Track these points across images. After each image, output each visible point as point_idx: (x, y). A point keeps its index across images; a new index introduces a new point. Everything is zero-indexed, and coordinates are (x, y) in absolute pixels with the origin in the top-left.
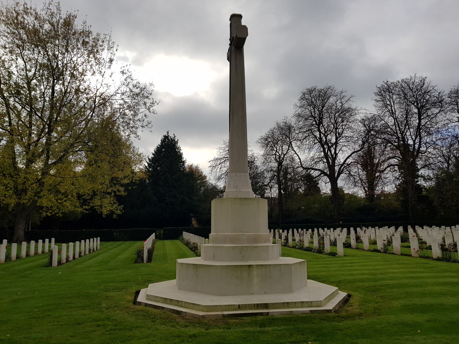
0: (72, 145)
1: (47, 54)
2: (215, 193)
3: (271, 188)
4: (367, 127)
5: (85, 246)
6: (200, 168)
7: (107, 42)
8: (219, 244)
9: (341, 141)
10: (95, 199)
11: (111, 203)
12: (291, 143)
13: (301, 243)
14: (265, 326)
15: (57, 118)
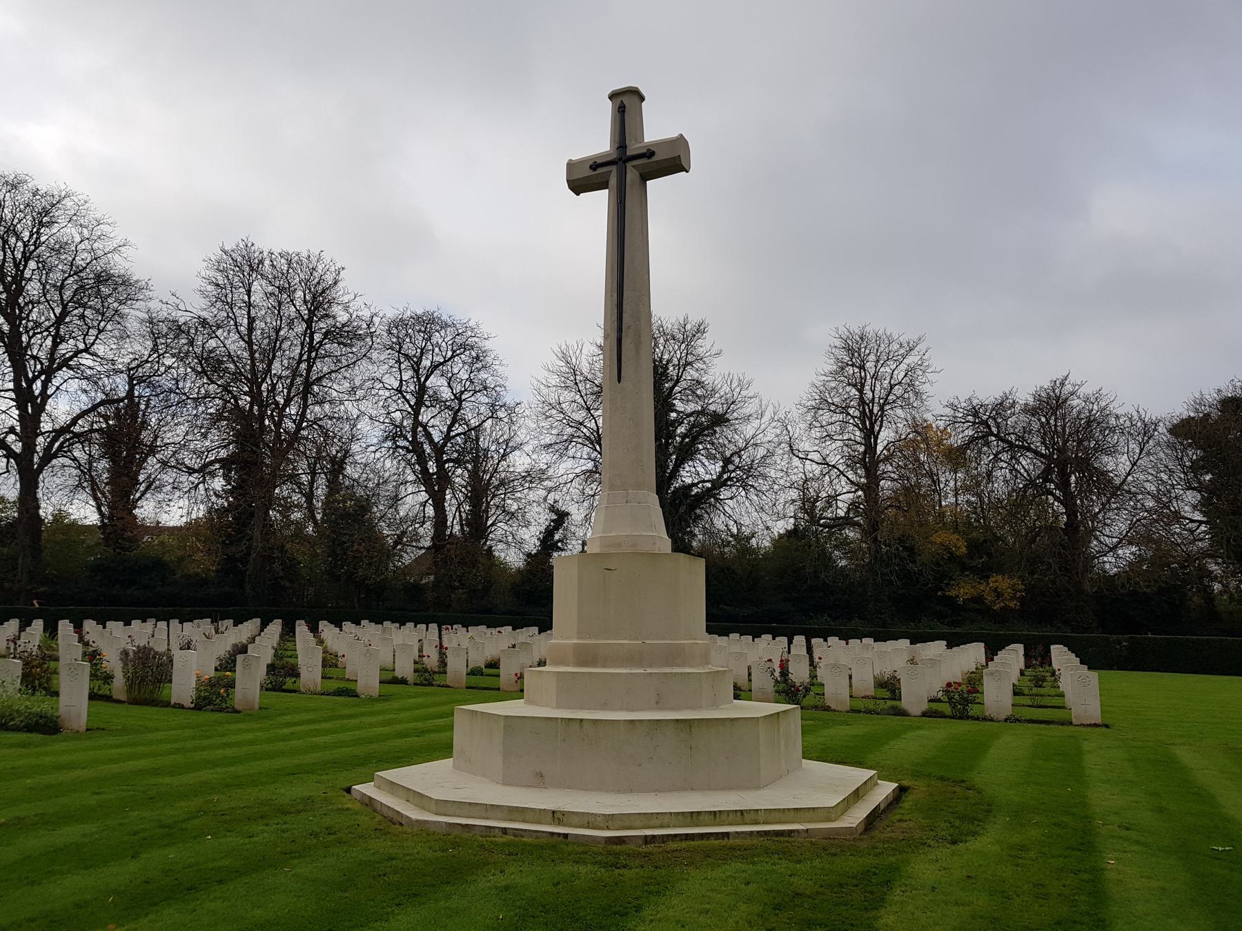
8: (604, 667)
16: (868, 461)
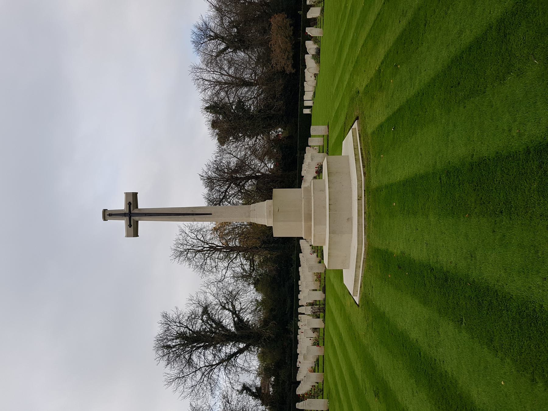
16: (228, 251)
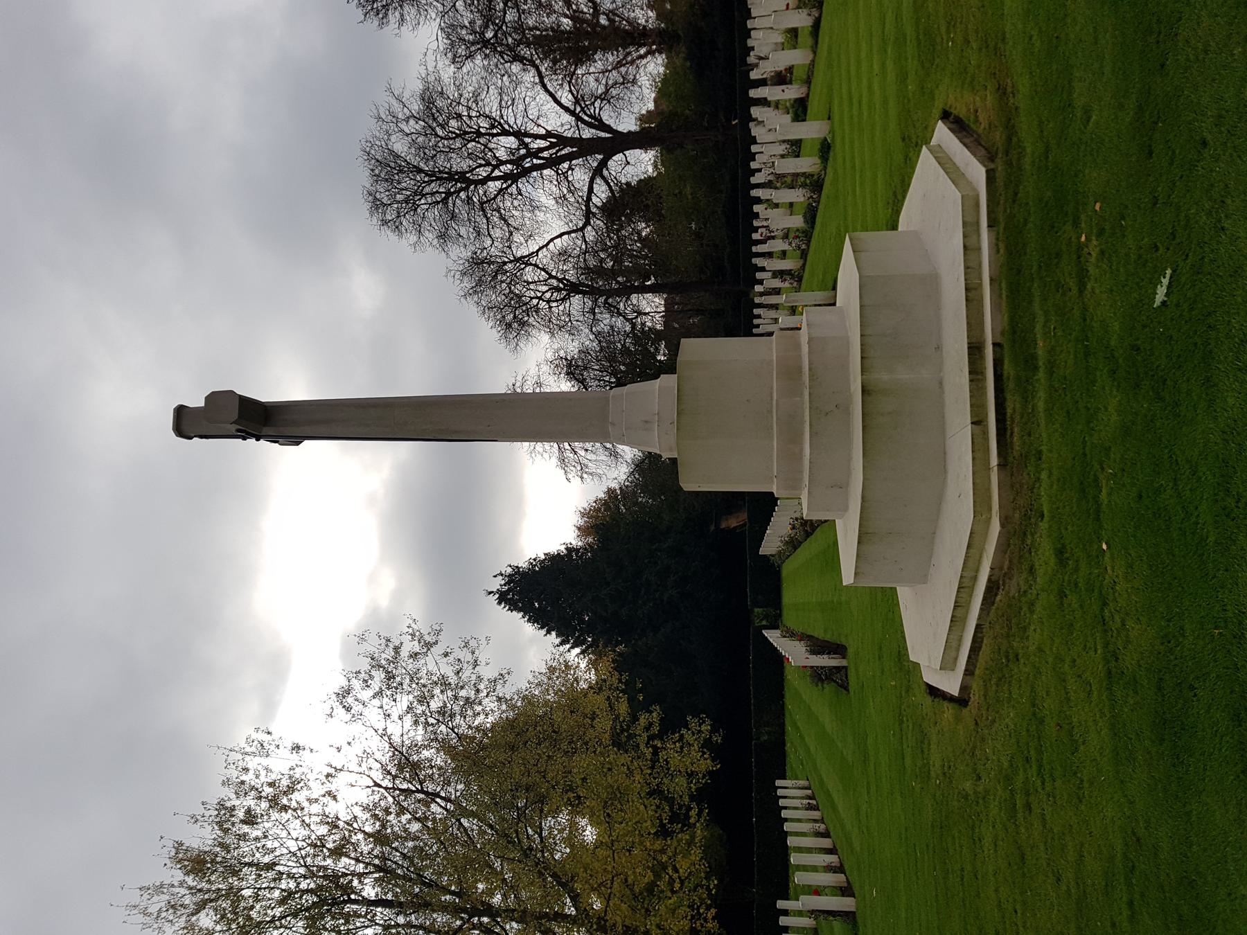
0: (527, 852)
1: (281, 918)
2: (655, 472)
3: (640, 313)
4: (473, 49)
5: (799, 821)
6: (586, 505)
7: (248, 758)
9: (511, 121)
10: (672, 790)
11: (682, 748)
12: (517, 260)
13: (791, 235)
14: (1034, 357)
15: (453, 893)
